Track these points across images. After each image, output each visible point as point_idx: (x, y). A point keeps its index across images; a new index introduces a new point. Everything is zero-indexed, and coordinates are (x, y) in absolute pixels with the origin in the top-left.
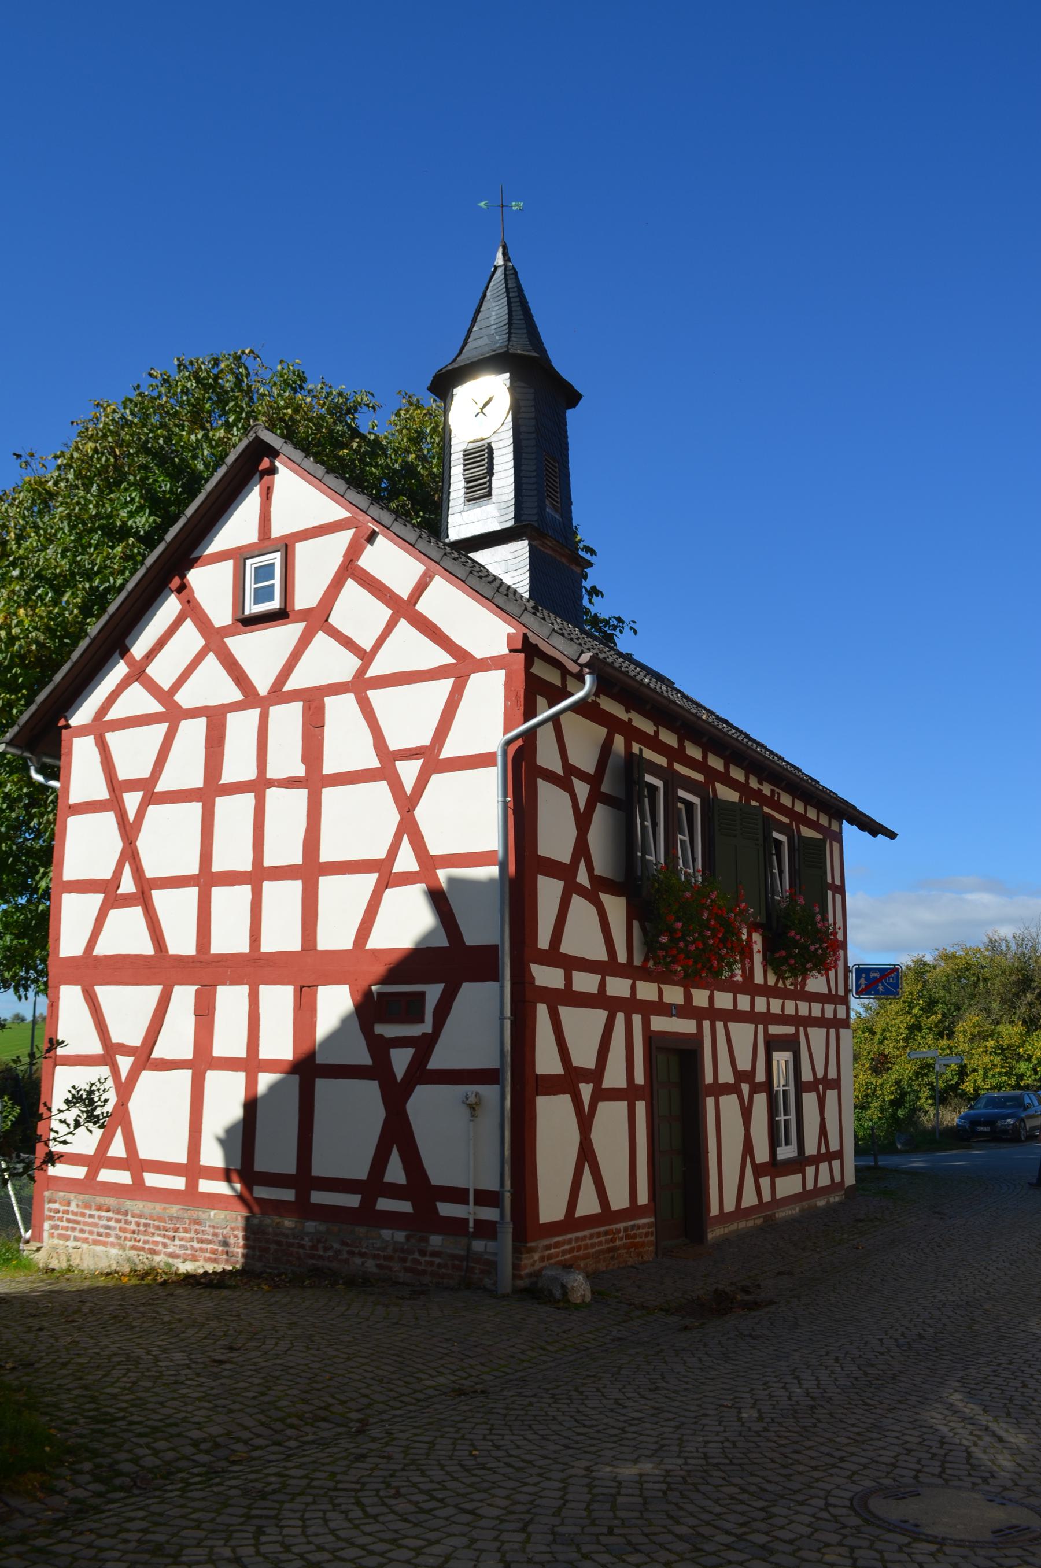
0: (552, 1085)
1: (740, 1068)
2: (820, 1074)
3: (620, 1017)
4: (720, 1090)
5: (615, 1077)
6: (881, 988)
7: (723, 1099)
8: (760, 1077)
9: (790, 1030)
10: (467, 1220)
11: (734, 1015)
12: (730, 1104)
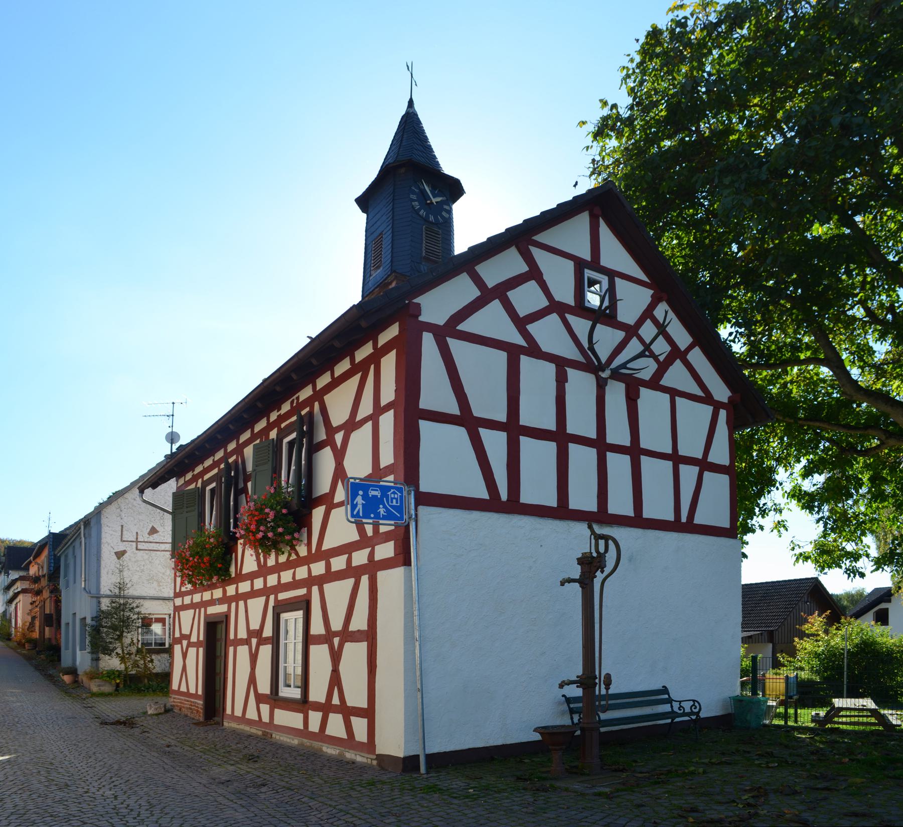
0: (319, 640)
1: (252, 628)
2: (337, 624)
3: (684, 519)
4: (238, 642)
5: (194, 639)
6: (382, 511)
7: (239, 648)
8: (268, 632)
9: (302, 592)
10: (418, 756)
11: (246, 596)
12: (243, 651)
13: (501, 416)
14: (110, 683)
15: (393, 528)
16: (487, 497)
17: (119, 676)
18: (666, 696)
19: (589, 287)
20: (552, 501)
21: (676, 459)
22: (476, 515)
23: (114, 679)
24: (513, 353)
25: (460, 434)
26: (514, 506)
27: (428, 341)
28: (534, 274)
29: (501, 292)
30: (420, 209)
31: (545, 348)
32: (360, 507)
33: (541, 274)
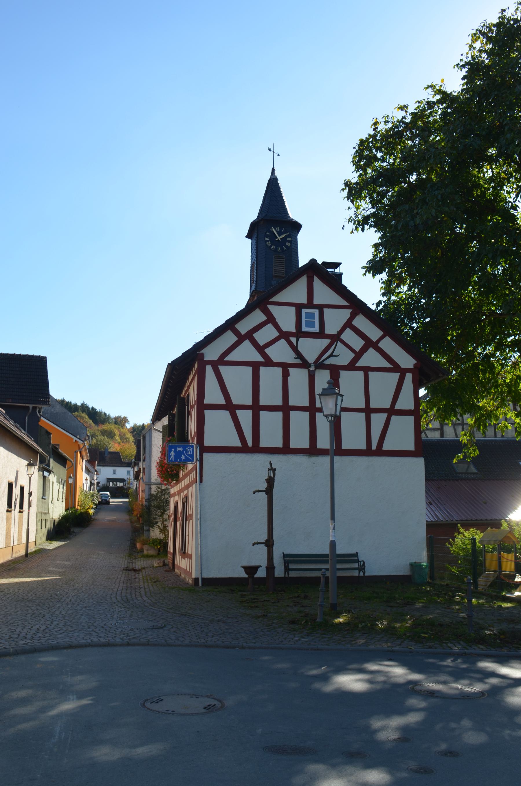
13: (249, 401)
14: (154, 548)
15: (85, 490)
16: (240, 445)
17: (160, 543)
18: (357, 558)
19: (49, 467)
20: (279, 444)
21: (368, 411)
22: (233, 455)
23: (156, 545)
24: (256, 366)
25: (226, 414)
26: (256, 449)
27: (209, 369)
28: (271, 320)
29: (250, 336)
30: (271, 246)
31: (275, 360)
32: (173, 456)
33: (275, 319)
